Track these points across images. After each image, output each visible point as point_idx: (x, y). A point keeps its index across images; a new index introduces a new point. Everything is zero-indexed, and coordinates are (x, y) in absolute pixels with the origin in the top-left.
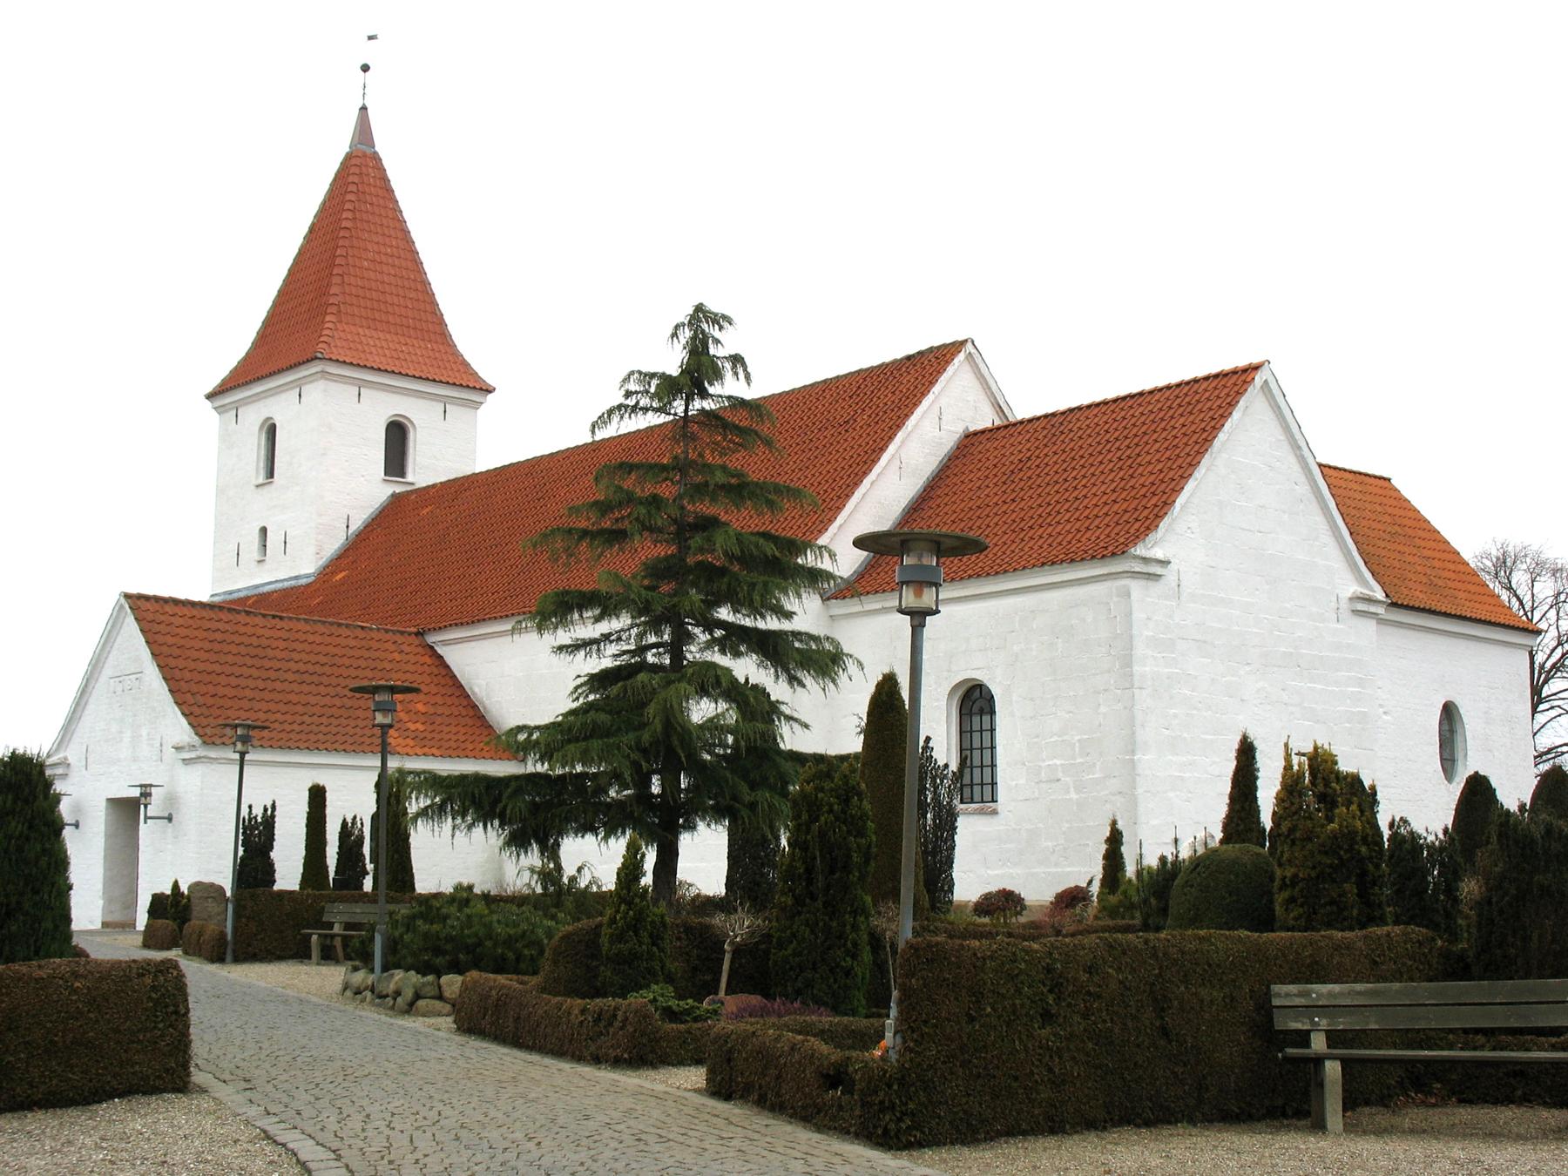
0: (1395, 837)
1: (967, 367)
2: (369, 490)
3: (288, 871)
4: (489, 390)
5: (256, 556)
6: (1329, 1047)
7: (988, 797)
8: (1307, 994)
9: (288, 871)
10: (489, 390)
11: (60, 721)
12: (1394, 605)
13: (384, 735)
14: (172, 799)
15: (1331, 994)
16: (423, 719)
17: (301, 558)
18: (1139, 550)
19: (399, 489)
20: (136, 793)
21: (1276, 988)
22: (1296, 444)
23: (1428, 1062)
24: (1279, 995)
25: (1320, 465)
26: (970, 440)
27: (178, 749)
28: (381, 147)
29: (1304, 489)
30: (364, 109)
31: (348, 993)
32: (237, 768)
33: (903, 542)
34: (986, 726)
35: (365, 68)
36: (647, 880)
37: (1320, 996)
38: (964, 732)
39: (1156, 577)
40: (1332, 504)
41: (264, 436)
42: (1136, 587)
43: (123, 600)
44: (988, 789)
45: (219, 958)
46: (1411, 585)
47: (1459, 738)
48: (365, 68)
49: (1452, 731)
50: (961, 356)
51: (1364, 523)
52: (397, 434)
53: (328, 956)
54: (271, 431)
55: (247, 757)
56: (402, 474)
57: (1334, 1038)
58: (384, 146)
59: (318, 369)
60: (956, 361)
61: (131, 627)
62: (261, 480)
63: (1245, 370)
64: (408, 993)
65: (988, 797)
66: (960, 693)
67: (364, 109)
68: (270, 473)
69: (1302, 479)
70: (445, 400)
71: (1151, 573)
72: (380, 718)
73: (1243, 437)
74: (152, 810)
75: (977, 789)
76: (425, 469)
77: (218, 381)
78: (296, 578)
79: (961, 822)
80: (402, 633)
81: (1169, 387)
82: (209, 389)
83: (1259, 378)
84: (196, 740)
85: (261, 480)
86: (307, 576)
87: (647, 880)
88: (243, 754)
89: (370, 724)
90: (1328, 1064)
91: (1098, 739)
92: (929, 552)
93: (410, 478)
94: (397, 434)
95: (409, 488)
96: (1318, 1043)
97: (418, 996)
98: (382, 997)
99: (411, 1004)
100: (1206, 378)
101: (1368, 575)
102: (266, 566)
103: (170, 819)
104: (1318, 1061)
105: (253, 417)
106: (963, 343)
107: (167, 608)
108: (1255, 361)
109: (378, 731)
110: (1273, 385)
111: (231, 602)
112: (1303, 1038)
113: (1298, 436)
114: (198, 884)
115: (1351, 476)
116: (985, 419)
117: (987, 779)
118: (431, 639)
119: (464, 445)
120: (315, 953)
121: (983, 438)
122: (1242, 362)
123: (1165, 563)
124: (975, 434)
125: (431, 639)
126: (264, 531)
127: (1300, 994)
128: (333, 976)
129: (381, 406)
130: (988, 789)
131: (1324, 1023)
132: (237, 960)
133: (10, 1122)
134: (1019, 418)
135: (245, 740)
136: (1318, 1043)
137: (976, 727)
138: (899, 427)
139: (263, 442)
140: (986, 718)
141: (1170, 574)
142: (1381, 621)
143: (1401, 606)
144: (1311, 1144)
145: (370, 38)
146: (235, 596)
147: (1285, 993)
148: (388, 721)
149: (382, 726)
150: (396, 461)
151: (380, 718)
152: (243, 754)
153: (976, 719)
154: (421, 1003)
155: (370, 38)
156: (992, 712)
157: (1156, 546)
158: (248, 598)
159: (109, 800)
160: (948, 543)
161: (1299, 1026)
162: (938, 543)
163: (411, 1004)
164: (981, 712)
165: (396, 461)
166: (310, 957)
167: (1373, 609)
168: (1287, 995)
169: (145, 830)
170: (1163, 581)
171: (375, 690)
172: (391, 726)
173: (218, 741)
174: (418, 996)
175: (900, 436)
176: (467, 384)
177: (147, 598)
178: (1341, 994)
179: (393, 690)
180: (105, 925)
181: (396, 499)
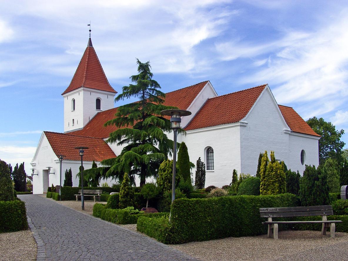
3: (76, 183)
5: (72, 125)
6: (273, 221)
7: (212, 169)
8: (267, 210)
13: (82, 157)
15: (273, 210)
16: (103, 155)
19: (99, 112)
20: (47, 169)
21: (260, 209)
22: (274, 101)
23: (292, 223)
24: (261, 210)
25: (278, 105)
26: (209, 100)
30: (90, 39)
32: (59, 164)
33: (172, 112)
34: (212, 155)
35: (90, 31)
37: (270, 210)
38: (208, 157)
39: (245, 126)
41: (73, 102)
43: (44, 133)
44: (212, 167)
46: (296, 128)
48: (90, 31)
50: (207, 84)
51: (287, 116)
52: (98, 101)
54: (74, 101)
57: (274, 219)
59: (82, 89)
61: (45, 139)
62: (73, 110)
65: (212, 169)
66: (207, 149)
67: (90, 39)
68: (74, 109)
70: (108, 95)
72: (81, 154)
75: (210, 167)
77: (64, 92)
78: (80, 129)
79: (206, 174)
80: (99, 139)
82: (62, 93)
83: (266, 87)
85: (73, 110)
86: (82, 128)
88: (61, 161)
89: (78, 155)
91: (224, 156)
92: (201, 122)
93: (101, 109)
94: (98, 101)
95: (101, 111)
96: (270, 220)
102: (74, 126)
104: (271, 224)
105: (70, 98)
106: (207, 81)
108: (265, 84)
111: (68, 133)
112: (267, 219)
113: (273, 99)
114: (57, 186)
115: (285, 107)
117: (212, 165)
121: (211, 100)
124: (210, 99)
127: (266, 210)
129: (96, 95)
130: (212, 167)
131: (271, 216)
132: (62, 200)
133: (5, 236)
136: (270, 220)
137: (210, 155)
138: (195, 98)
140: (212, 154)
141: (248, 126)
142: (290, 134)
144: (270, 241)
145: (89, 25)
146: (69, 132)
147: (262, 210)
149: (81, 155)
150: (98, 107)
151: (81, 154)
152: (61, 161)
153: (210, 154)
155: (89, 25)
156: (213, 153)
158: (71, 133)
159: (43, 170)
160: (182, 112)
161: (266, 217)
162: (180, 113)
164: (211, 153)
165: (98, 107)
166: (76, 200)
168: (263, 210)
169: (50, 175)
170: (246, 127)
172: (83, 155)
173: (90, 160)
175: (195, 99)
177: (48, 132)
178: (275, 210)
179: (83, 148)
180: (44, 193)
181: (98, 114)
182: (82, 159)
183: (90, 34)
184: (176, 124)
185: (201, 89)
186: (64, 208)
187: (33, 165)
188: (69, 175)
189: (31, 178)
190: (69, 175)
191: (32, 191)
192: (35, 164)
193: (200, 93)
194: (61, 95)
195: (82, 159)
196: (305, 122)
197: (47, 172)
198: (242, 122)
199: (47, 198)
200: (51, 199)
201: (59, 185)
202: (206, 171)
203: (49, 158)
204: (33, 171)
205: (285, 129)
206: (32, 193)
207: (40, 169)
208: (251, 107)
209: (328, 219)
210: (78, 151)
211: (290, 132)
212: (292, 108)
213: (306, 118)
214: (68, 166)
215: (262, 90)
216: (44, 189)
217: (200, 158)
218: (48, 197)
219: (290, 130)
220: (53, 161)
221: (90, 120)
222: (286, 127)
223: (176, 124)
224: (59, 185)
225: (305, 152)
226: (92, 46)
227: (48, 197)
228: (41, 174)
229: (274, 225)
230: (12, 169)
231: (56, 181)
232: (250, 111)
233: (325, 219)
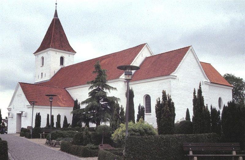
0: (91, 96)
1: (146, 47)
2: (58, 67)
3: (43, 124)
4: (76, 53)
5: (41, 77)
6: (236, 154)
9: (43, 124)
10: (76, 53)
11: (10, 102)
12: (211, 83)
14: (26, 113)
17: (47, 77)
18: (172, 74)
20: (21, 113)
22: (196, 58)
25: (200, 62)
26: (147, 58)
27: (27, 106)
28: (59, 17)
29: (197, 65)
30: (56, 10)
31: (46, 144)
32: (50, 109)
33: (126, 68)
35: (56, 4)
36: (55, 126)
38: (146, 102)
40: (202, 67)
42: (171, 80)
45: (30, 138)
47: (221, 103)
48: (56, 4)
49: (220, 102)
50: (145, 46)
52: (62, 59)
53: (43, 138)
54: (43, 58)
55: (34, 107)
56: (63, 65)
58: (60, 17)
60: (144, 46)
63: (188, 47)
64: (54, 144)
66: (146, 96)
67: (56, 10)
68: (43, 65)
69: (197, 64)
71: (174, 78)
72: (50, 100)
73: (188, 58)
74: (23, 115)
76: (66, 64)
81: (177, 50)
83: (190, 48)
84: (30, 105)
86: (48, 80)
87: (55, 126)
88: (33, 106)
90: (195, 157)
93: (64, 65)
94: (62, 59)
96: (191, 153)
97: (56, 144)
98: (51, 144)
99: (55, 146)
100: (182, 48)
101: (207, 78)
103: (26, 116)
105: (40, 56)
106: (145, 44)
107: (28, 85)
109: (50, 102)
110: (192, 49)
116: (149, 55)
118: (66, 89)
119: (70, 60)
120: (41, 137)
122: (188, 46)
123: (176, 76)
124: (147, 57)
125: (66, 89)
126: (42, 73)
128: (44, 141)
134: (154, 55)
135: (34, 104)
139: (42, 61)
143: (212, 83)
146: (38, 83)
148: (51, 100)
151: (50, 100)
152: (33, 106)
154: (56, 145)
157: (176, 73)
159: (17, 114)
163: (55, 146)
167: (208, 83)
169: (22, 118)
171: (50, 95)
174: (56, 144)
175: (136, 57)
176: (71, 50)
179: (52, 95)
181: (62, 68)
182: (51, 105)
183: (56, 7)
184: (128, 77)
185: (141, 50)
186: (35, 144)
187: (9, 109)
188: (38, 118)
189: (7, 121)
190: (38, 118)
191: (7, 131)
192: (11, 108)
193: (140, 52)
194: (77, 52)
195: (51, 105)
196: (222, 76)
197: (20, 115)
198: (173, 75)
199: (21, 137)
200: (24, 138)
201: (31, 126)
202: (145, 113)
203: (22, 103)
204: (9, 114)
205: (206, 80)
206: (7, 133)
207: (15, 113)
208: (179, 63)
209: (237, 153)
210: (48, 98)
211: (209, 83)
212: (210, 64)
213: (223, 73)
214: (37, 110)
215: (187, 51)
216: (17, 128)
217: (140, 104)
218: (21, 136)
219: (209, 81)
220: (26, 106)
221: (55, 73)
222: (206, 79)
223: (128, 77)
224: (31, 126)
225: (222, 99)
226: (58, 17)
227: (21, 136)
228: (15, 117)
229: (194, 158)
230: (135, 113)
231: (28, 123)
232: (179, 67)
233: (234, 153)
